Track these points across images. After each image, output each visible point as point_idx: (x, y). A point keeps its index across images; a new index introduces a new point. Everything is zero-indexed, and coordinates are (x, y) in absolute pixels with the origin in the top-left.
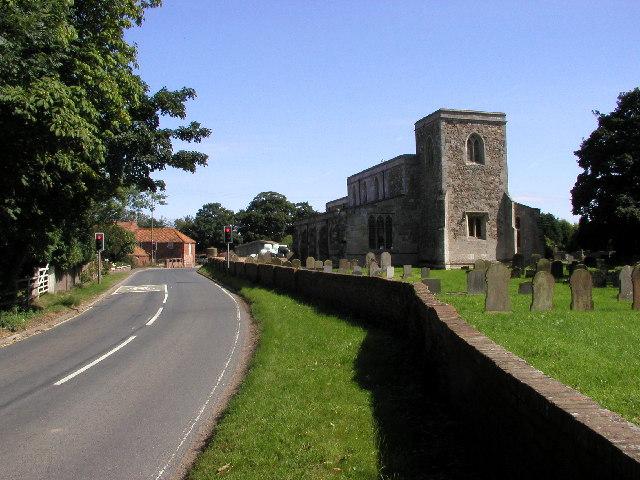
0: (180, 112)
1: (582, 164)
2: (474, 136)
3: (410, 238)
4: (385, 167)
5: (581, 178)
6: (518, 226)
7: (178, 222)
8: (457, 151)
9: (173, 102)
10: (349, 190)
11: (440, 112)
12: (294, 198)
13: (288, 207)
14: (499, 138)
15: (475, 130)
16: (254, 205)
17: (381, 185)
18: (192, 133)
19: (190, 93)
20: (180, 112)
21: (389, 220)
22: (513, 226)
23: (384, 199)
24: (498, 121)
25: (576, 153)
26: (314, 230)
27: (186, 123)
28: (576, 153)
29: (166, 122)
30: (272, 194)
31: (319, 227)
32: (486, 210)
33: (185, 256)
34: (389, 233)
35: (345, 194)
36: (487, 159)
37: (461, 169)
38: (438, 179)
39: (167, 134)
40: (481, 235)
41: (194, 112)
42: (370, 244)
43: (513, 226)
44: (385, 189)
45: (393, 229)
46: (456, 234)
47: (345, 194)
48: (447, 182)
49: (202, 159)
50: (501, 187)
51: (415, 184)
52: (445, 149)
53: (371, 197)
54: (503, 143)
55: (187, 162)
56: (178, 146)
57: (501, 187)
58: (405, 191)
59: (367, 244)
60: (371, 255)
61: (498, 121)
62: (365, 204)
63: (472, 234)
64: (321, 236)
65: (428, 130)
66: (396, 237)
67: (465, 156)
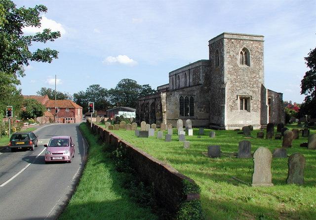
0: (37, 23)
1: (309, 65)
2: (244, 49)
3: (204, 110)
4: (190, 67)
5: (308, 74)
6: (269, 103)
7: (75, 95)
8: (232, 57)
9: (32, 16)
10: (210, 52)
11: (223, 34)
12: (141, 82)
13: (139, 87)
14: (259, 51)
15: (245, 46)
16: (119, 85)
17: (188, 77)
18: (46, 36)
19: (44, 9)
20: (37, 23)
21: (192, 99)
22: (267, 104)
23: (189, 86)
24: (259, 40)
25: (306, 59)
26: (148, 103)
27: (40, 30)
28: (306, 59)
29: (28, 30)
30: (129, 80)
31: (151, 102)
32: (251, 94)
33: (76, 116)
34: (192, 107)
35: (207, 57)
36: (252, 63)
37: (236, 70)
38: (222, 75)
39: (29, 39)
40: (247, 108)
41: (47, 23)
42: (180, 113)
43: (267, 104)
44: (190, 80)
45: (195, 104)
46: (232, 108)
47: (207, 57)
48: (227, 78)
49: (55, 54)
50: (260, 80)
51: (208, 78)
52: (226, 57)
53: (182, 85)
54: (262, 54)
55: (44, 56)
56: (34, 47)
57: (260, 80)
58: (202, 82)
59: (179, 113)
60: (180, 122)
61: (259, 40)
62: (179, 89)
63: (242, 108)
64: (152, 108)
65: (216, 45)
66: (196, 110)
67: (238, 62)
